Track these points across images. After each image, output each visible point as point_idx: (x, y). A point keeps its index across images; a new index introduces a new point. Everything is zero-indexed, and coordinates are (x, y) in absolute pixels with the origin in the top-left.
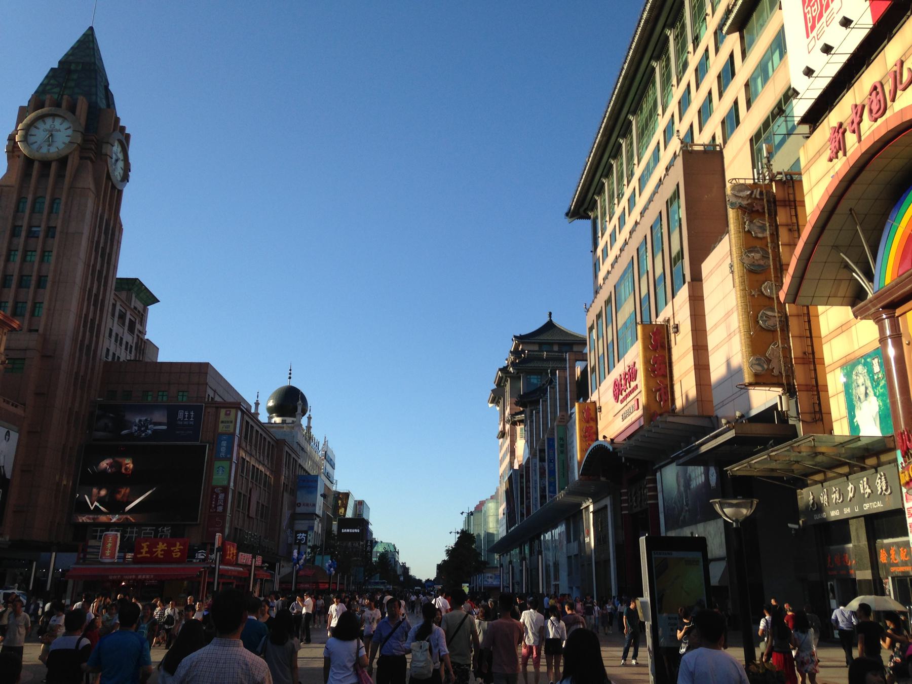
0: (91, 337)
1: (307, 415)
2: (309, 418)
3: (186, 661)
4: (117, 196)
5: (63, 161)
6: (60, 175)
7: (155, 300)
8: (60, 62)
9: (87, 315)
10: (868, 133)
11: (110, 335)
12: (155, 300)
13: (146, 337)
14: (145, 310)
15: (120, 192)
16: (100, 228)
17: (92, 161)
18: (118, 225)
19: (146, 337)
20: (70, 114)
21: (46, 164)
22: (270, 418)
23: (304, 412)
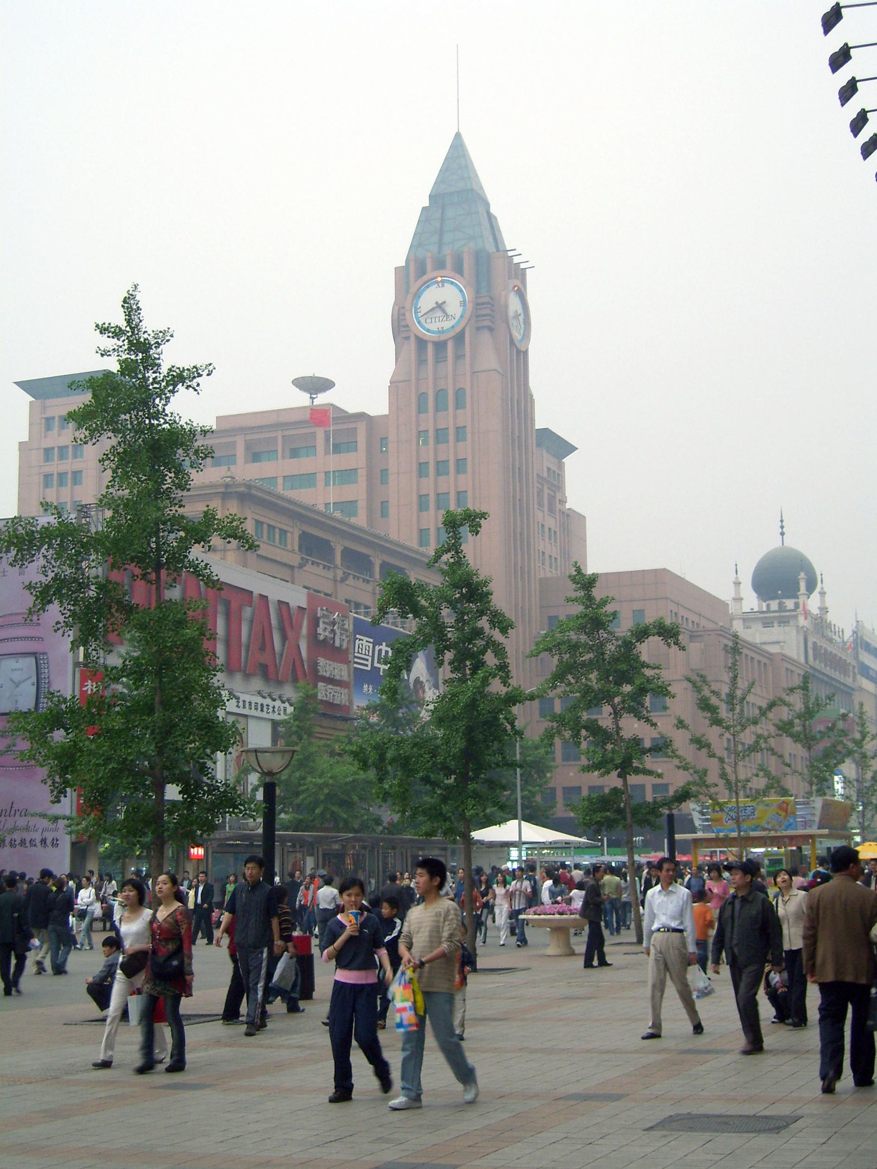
0: (522, 521)
1: (818, 589)
2: (823, 594)
3: (652, 939)
4: (522, 356)
5: (459, 338)
6: (459, 357)
7: (573, 449)
8: (431, 197)
9: (514, 497)
10: (352, 677)
11: (543, 532)
12: (573, 449)
13: (568, 506)
14: (561, 466)
15: (526, 353)
16: (513, 415)
17: (491, 329)
18: (529, 397)
19: (568, 506)
20: (457, 275)
21: (440, 346)
22: (242, 1023)
23: (811, 586)
